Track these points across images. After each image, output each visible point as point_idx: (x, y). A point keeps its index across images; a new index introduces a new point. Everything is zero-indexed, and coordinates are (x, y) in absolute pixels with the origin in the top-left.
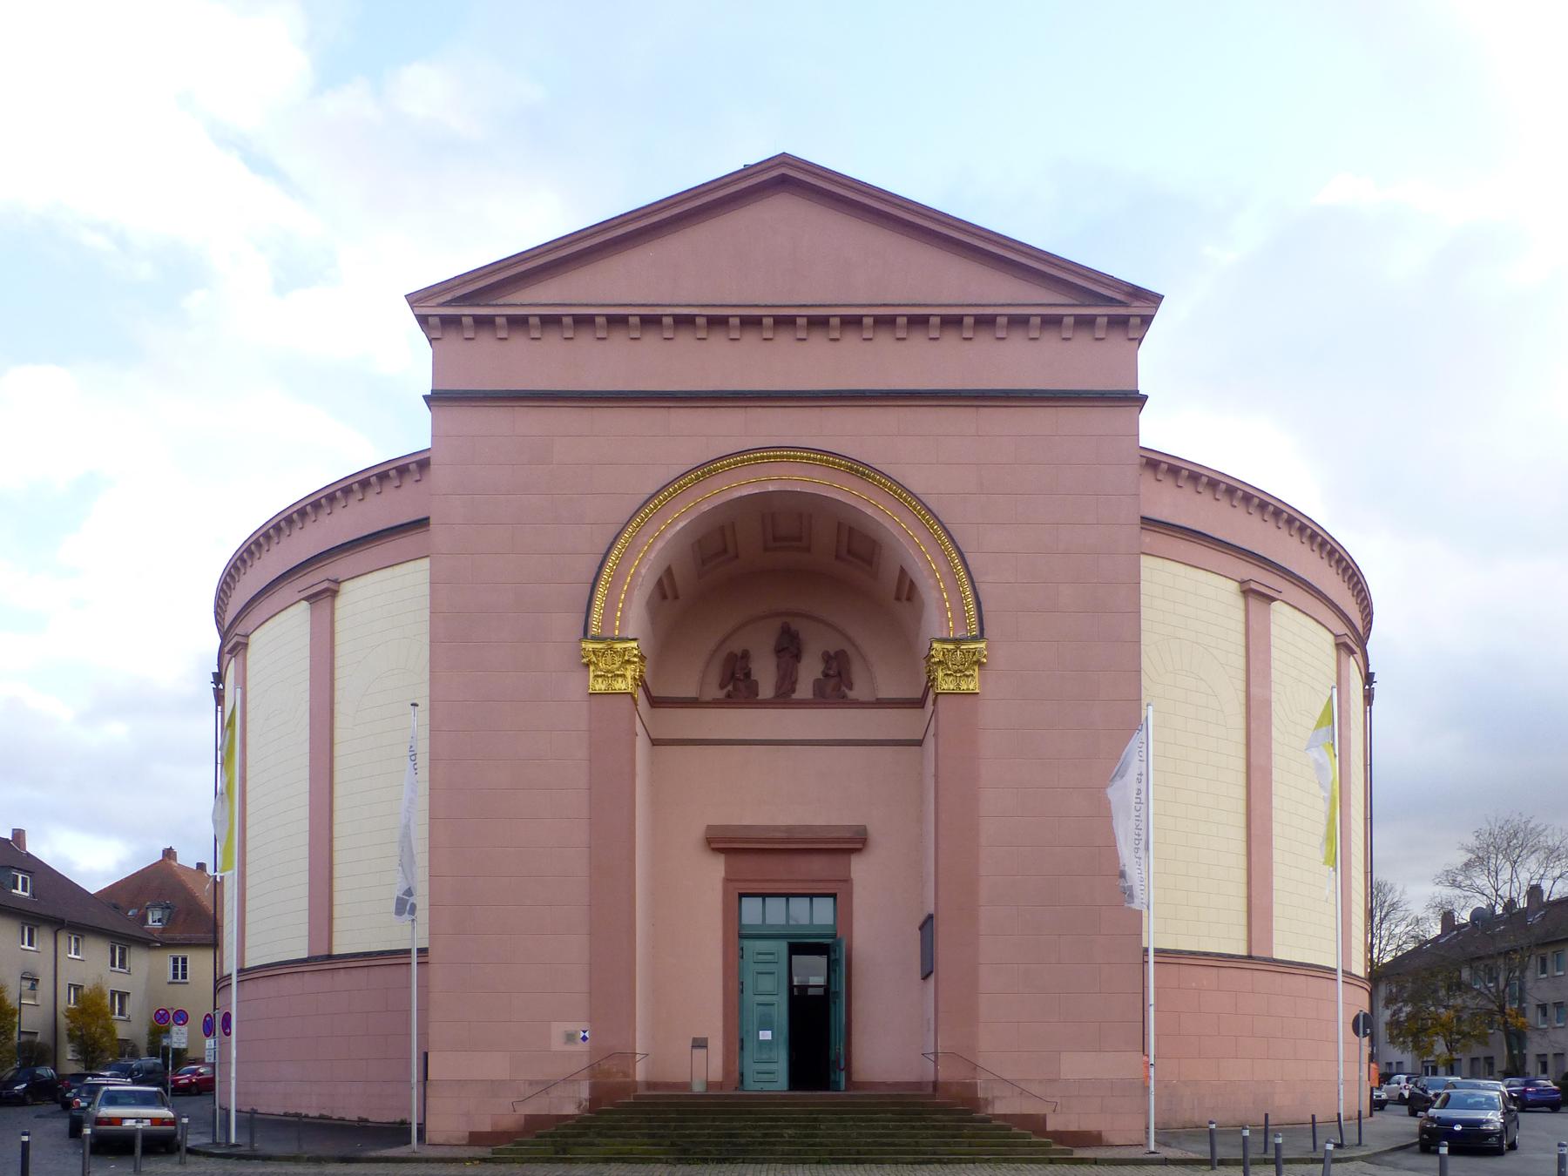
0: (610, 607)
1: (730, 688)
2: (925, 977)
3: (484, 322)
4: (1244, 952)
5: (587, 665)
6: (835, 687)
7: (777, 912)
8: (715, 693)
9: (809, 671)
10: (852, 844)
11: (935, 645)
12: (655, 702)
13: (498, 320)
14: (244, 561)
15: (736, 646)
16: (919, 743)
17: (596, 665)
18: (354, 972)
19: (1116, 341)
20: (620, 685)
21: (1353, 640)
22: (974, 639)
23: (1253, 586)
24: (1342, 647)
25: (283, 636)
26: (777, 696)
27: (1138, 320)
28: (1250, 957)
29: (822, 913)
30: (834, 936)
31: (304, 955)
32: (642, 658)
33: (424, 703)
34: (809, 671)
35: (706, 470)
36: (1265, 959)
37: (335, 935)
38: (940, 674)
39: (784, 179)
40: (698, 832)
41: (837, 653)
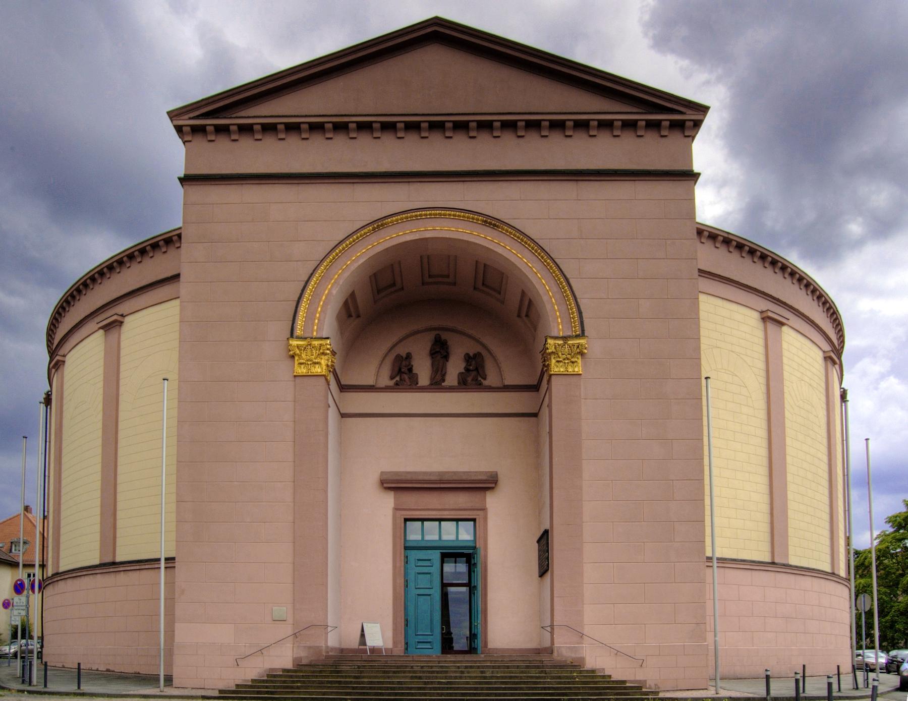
0: (310, 318)
1: (398, 378)
2: (542, 574)
3: (222, 130)
4: (768, 560)
5: (293, 357)
6: (473, 377)
7: (432, 533)
8: (385, 381)
9: (454, 368)
10: (485, 485)
11: (549, 341)
12: (343, 388)
13: (232, 128)
14: (60, 314)
15: (402, 350)
16: (535, 415)
17: (300, 356)
18: (130, 573)
19: (675, 140)
20: (317, 370)
21: (834, 355)
22: (577, 336)
23: (770, 314)
24: (827, 358)
25: (87, 354)
26: (431, 384)
27: (691, 123)
28: (773, 563)
29: (465, 534)
30: (475, 548)
31: (97, 562)
32: (334, 353)
33: (174, 376)
34: (454, 368)
35: (379, 224)
36: (784, 565)
37: (117, 549)
38: (553, 361)
39: (437, 34)
40: (373, 477)
41: (475, 355)
